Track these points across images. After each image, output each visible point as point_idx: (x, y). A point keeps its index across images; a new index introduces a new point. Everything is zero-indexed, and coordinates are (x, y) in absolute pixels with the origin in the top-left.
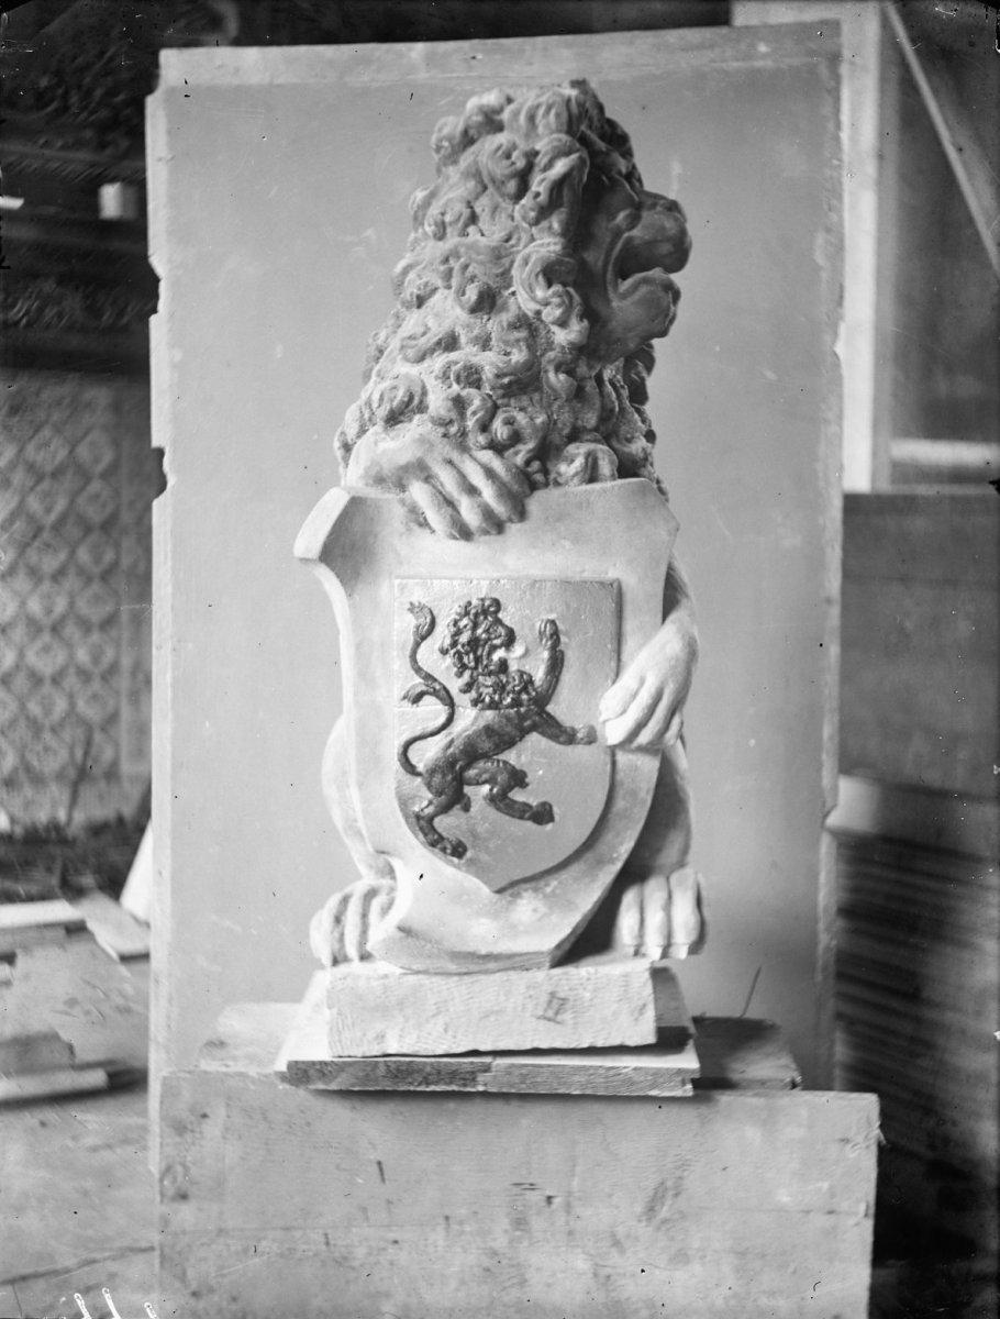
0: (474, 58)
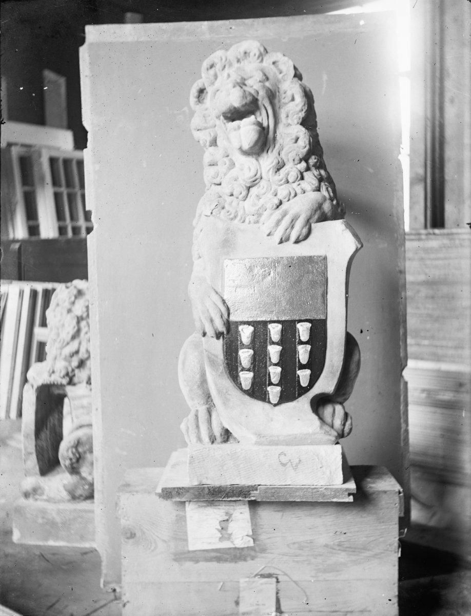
0: (231, 28)
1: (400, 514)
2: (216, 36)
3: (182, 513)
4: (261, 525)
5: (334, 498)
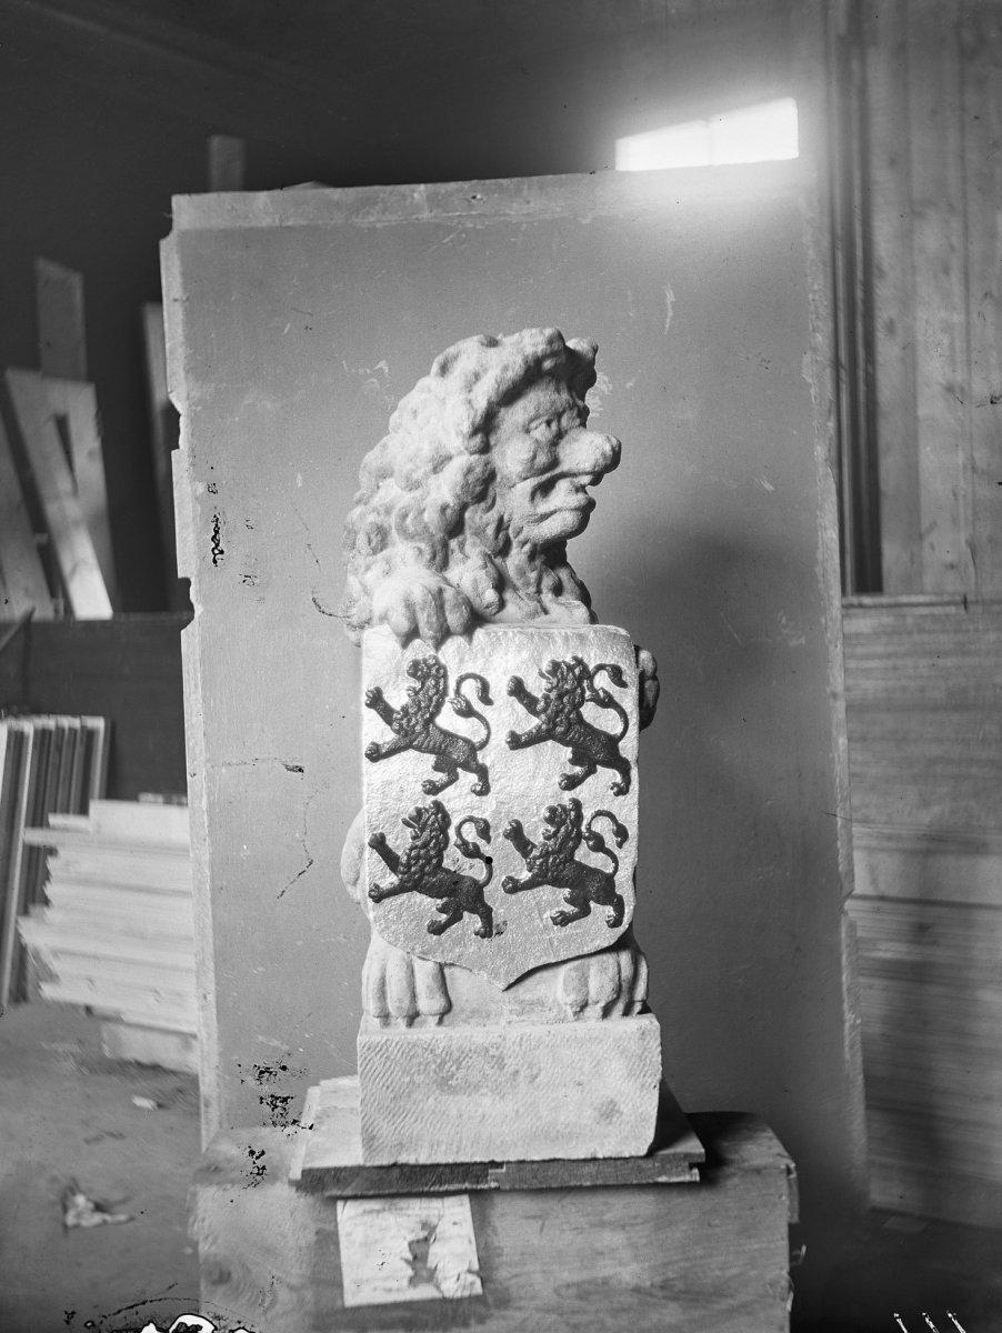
0: (474, 198)
1: (791, 1217)
2: (445, 215)
5: (660, 1175)
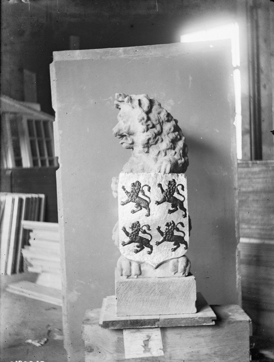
0: (136, 51)
2: (128, 56)
3: (121, 336)
4: (168, 343)
5: (204, 323)
